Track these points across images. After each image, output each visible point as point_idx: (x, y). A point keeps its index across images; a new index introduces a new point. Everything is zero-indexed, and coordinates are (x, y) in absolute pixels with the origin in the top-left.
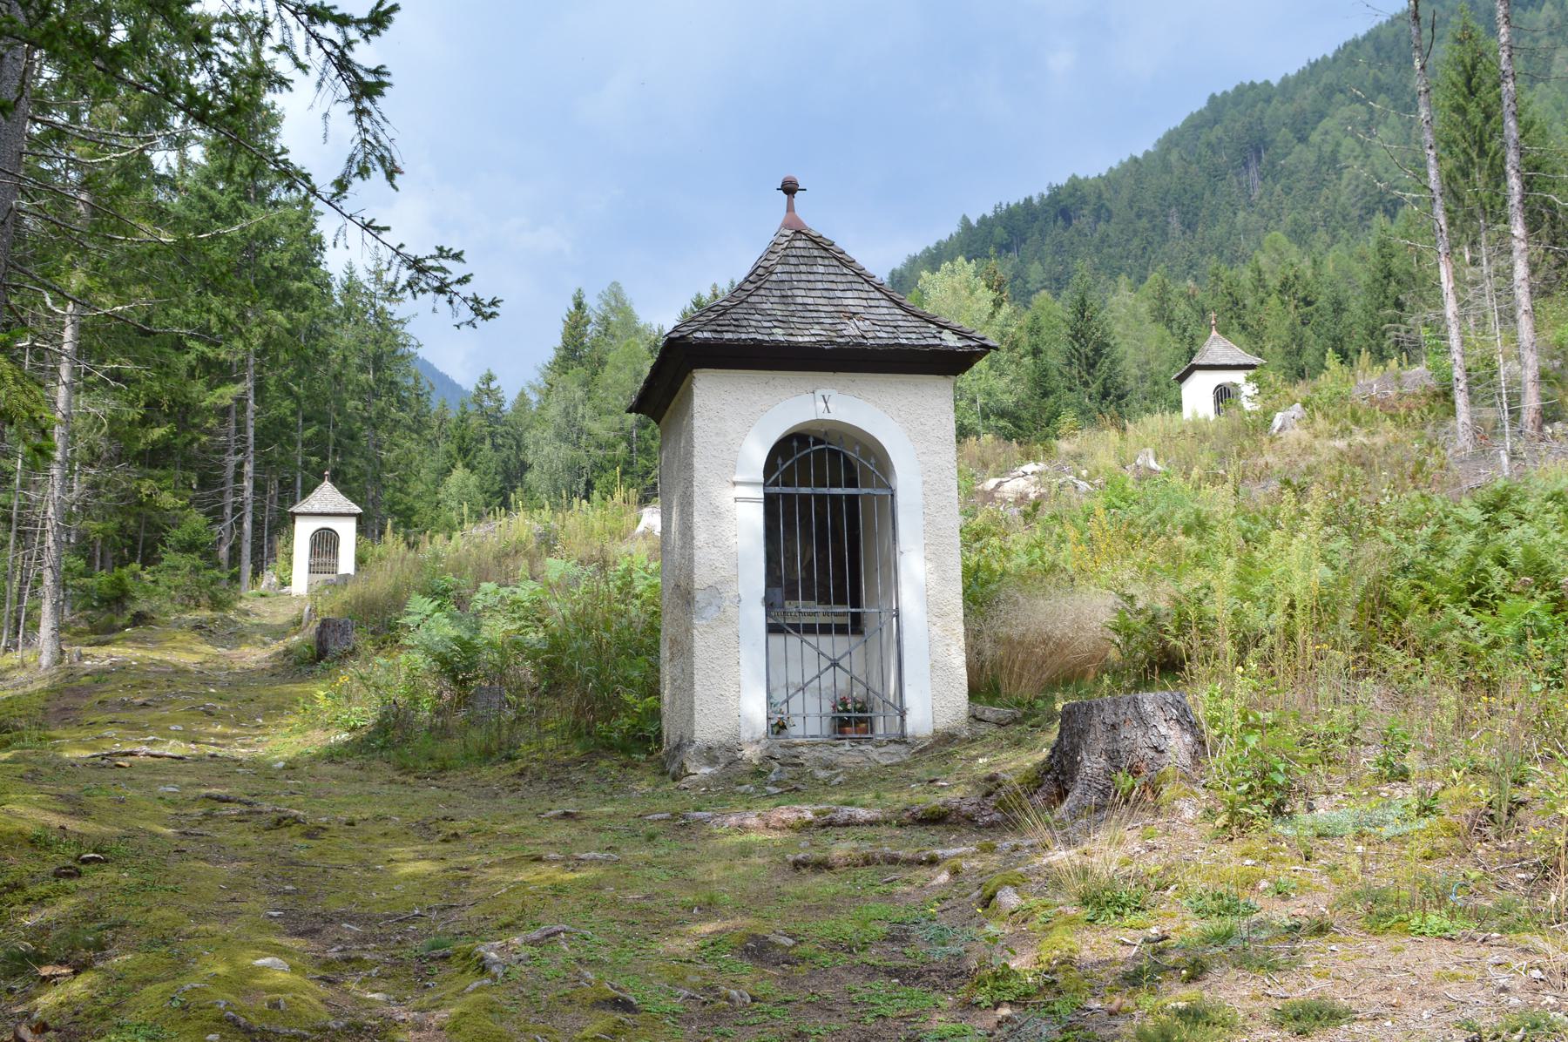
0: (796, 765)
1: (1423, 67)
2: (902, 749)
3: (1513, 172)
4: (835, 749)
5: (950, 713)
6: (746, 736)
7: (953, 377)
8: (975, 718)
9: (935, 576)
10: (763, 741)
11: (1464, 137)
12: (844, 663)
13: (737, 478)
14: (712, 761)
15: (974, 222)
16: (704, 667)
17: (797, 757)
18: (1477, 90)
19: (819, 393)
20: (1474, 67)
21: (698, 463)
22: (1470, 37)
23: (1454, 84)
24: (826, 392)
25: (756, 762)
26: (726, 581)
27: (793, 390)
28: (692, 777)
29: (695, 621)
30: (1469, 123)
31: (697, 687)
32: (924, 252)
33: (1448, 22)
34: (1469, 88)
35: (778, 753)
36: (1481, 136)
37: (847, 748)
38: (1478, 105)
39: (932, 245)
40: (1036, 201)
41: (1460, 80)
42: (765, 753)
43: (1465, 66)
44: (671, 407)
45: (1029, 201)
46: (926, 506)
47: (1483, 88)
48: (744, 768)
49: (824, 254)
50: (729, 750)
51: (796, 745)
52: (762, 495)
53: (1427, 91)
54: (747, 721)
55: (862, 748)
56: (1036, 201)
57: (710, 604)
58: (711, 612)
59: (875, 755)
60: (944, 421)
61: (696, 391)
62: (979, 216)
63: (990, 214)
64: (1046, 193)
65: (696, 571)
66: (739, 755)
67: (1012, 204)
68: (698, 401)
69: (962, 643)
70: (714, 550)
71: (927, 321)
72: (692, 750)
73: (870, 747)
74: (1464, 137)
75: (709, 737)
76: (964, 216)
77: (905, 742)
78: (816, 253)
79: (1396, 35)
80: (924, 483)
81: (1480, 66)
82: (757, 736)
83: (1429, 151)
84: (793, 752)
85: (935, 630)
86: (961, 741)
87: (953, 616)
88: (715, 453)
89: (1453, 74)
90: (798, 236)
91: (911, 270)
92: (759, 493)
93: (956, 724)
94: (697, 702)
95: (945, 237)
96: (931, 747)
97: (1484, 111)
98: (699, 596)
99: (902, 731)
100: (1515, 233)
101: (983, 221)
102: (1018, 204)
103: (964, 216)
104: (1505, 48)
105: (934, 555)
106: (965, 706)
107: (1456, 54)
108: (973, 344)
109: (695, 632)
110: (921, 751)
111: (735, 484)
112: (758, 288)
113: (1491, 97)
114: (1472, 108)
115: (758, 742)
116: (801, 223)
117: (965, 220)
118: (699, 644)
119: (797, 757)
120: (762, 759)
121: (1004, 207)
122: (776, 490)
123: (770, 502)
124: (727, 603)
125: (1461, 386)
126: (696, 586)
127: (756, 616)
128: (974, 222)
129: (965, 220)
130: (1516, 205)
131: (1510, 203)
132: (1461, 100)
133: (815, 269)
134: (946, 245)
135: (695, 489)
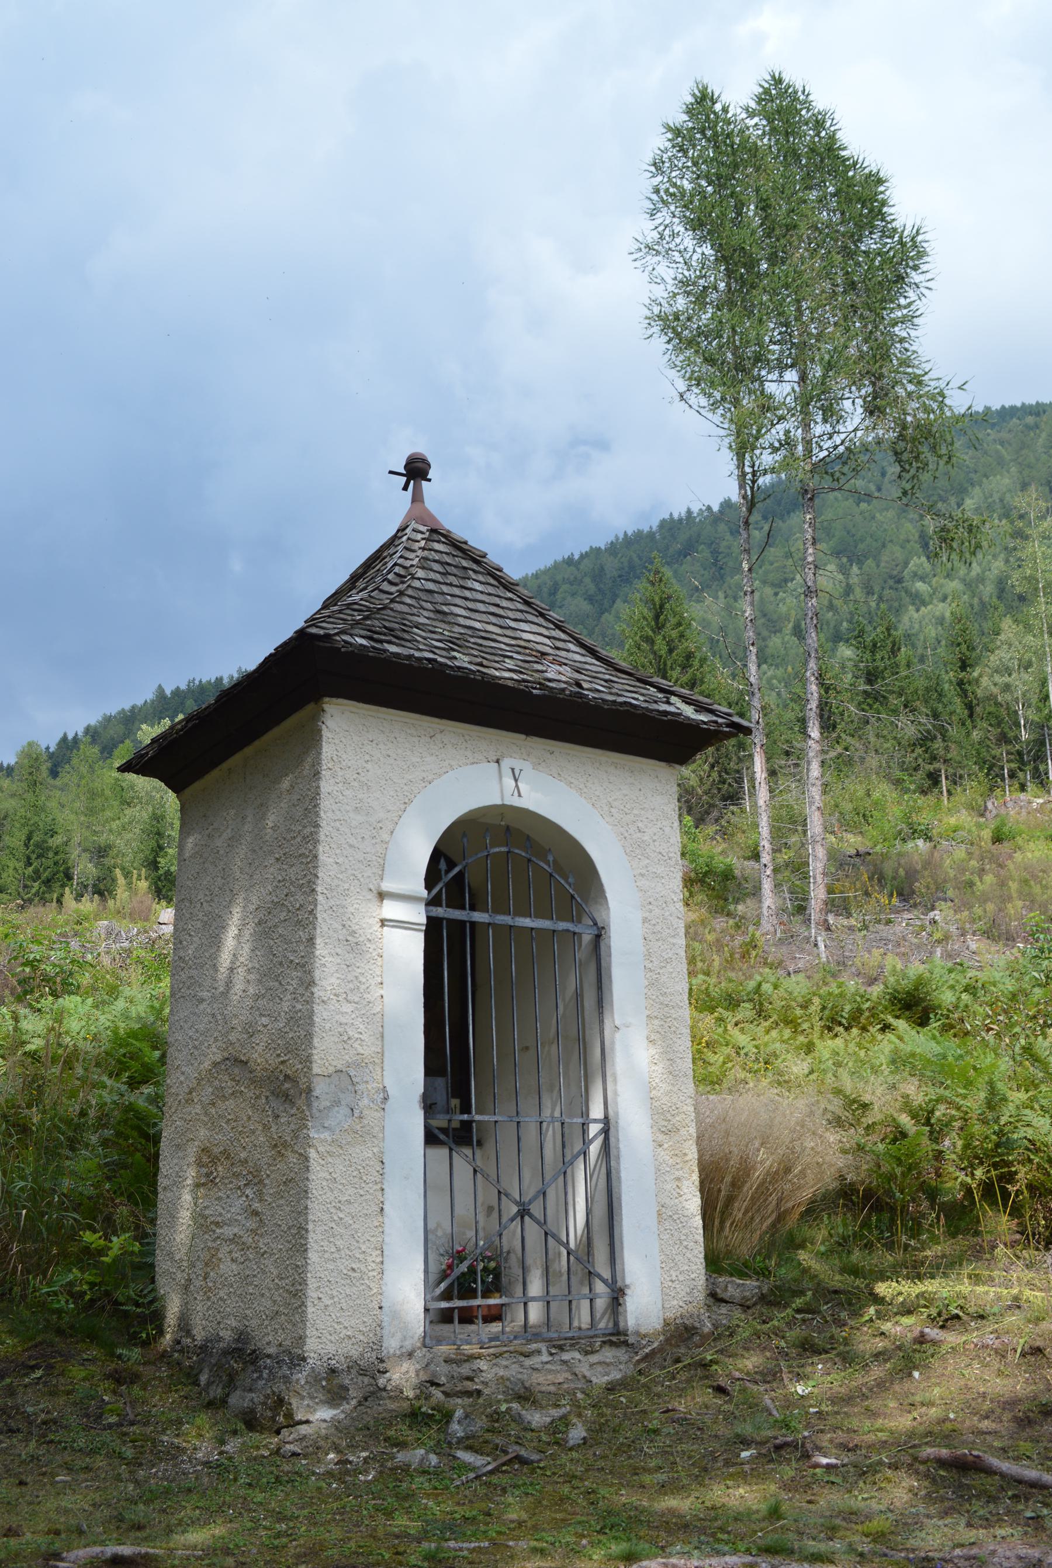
0: (468, 1394)
1: (750, 570)
2: (621, 1354)
3: (813, 679)
4: (528, 1362)
5: (682, 1291)
6: (392, 1344)
7: (677, 766)
8: (715, 1297)
9: (659, 1068)
10: (419, 1354)
11: (651, 663)
12: (536, 1209)
13: (387, 886)
14: (336, 1395)
15: (168, 692)
16: (326, 1217)
17: (470, 1379)
18: (663, 626)
19: (507, 763)
20: (662, 606)
21: (326, 856)
22: (661, 580)
23: (644, 618)
24: (518, 764)
25: (411, 1394)
26: (360, 1063)
27: (469, 753)
28: (303, 1429)
29: (312, 1134)
30: (655, 653)
31: (313, 1256)
32: (119, 713)
33: (581, 581)
34: (657, 623)
35: (442, 1371)
36: (665, 664)
37: (545, 1357)
38: (664, 638)
39: (127, 707)
40: (226, 681)
41: (650, 615)
42: (424, 1377)
43: (655, 605)
44: (225, 766)
45: (219, 680)
46: (648, 955)
47: (668, 625)
48: (392, 1406)
49: (475, 567)
50: (363, 1372)
51: (471, 1358)
52: (423, 920)
53: (752, 592)
54: (396, 1315)
55: (566, 1356)
56: (226, 681)
57: (337, 1103)
58: (339, 1116)
59: (584, 1369)
60: (667, 829)
61: (326, 733)
62: (173, 688)
63: (183, 687)
64: (236, 676)
65: (316, 1041)
66: (381, 1382)
67: (204, 681)
68: (328, 750)
69: (695, 1177)
70: (347, 1008)
71: (639, 680)
72: (301, 1377)
73: (577, 1355)
74: (651, 663)
75: (331, 1349)
76: (160, 686)
77: (626, 1343)
78: (465, 563)
79: (539, 587)
80: (645, 920)
81: (667, 606)
82: (408, 1345)
83: (751, 648)
84: (465, 1370)
85: (664, 1155)
86: (704, 1337)
87: (683, 1132)
88: (352, 841)
89: (645, 611)
90: (435, 537)
91: (105, 728)
92: (418, 915)
93: (690, 1308)
94: (312, 1283)
95: (139, 702)
96: (660, 1350)
97: (668, 644)
98: (320, 1088)
99: (616, 1324)
100: (813, 735)
101: (177, 692)
102: (209, 682)
103: (160, 686)
104: (812, 566)
105: (661, 1036)
106: (701, 1281)
107: (648, 594)
108: (720, 720)
109: (312, 1154)
110: (646, 1357)
111: (382, 896)
112: (401, 593)
113: (674, 634)
114: (659, 639)
115: (410, 1355)
116: (437, 521)
117: (160, 690)
118: (318, 1174)
119: (470, 1379)
120: (421, 1386)
121: (197, 682)
122: (440, 912)
123: (433, 930)
124: (365, 1101)
125: (768, 872)
126: (316, 1070)
127: (416, 1123)
128: (168, 692)
129: (160, 690)
130: (814, 709)
131: (809, 707)
132: (650, 633)
133: (469, 584)
134: (140, 709)
135: (320, 898)
